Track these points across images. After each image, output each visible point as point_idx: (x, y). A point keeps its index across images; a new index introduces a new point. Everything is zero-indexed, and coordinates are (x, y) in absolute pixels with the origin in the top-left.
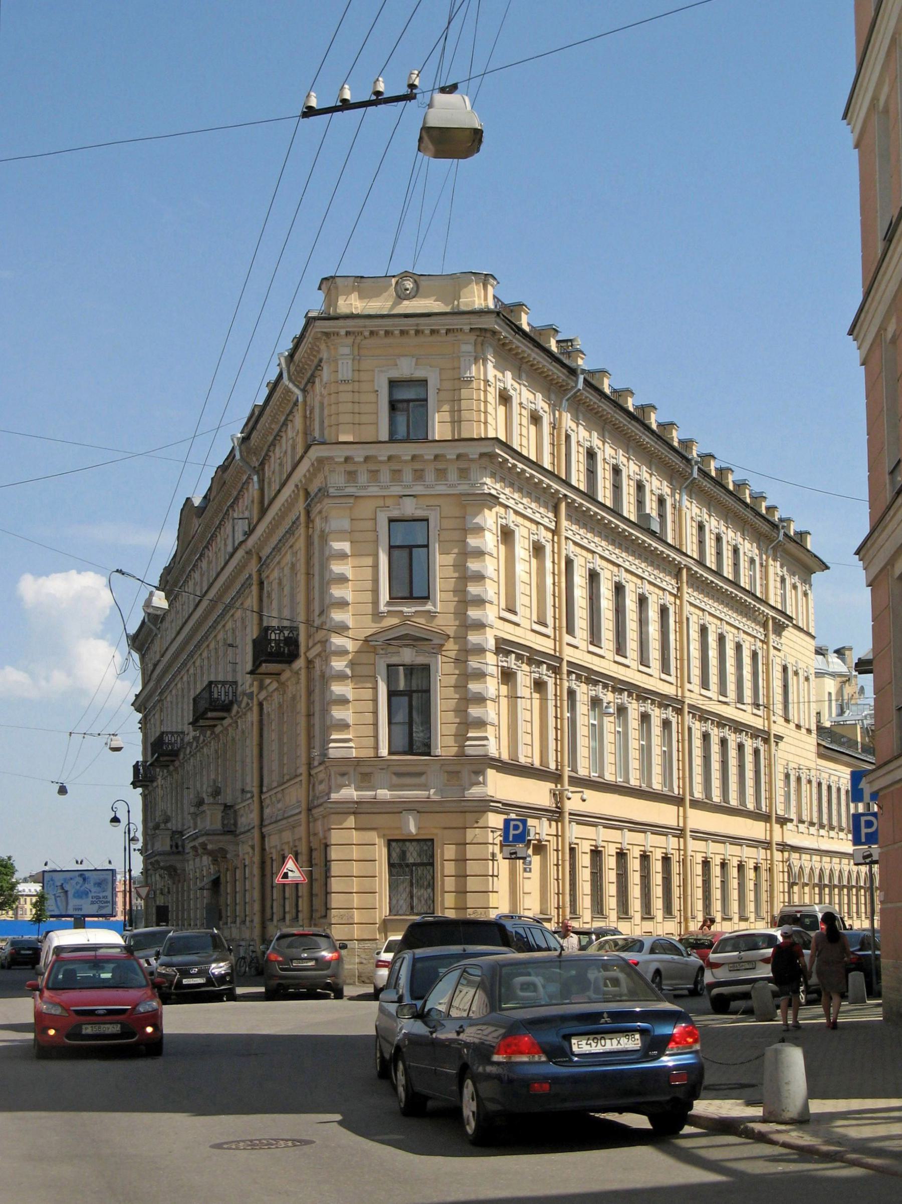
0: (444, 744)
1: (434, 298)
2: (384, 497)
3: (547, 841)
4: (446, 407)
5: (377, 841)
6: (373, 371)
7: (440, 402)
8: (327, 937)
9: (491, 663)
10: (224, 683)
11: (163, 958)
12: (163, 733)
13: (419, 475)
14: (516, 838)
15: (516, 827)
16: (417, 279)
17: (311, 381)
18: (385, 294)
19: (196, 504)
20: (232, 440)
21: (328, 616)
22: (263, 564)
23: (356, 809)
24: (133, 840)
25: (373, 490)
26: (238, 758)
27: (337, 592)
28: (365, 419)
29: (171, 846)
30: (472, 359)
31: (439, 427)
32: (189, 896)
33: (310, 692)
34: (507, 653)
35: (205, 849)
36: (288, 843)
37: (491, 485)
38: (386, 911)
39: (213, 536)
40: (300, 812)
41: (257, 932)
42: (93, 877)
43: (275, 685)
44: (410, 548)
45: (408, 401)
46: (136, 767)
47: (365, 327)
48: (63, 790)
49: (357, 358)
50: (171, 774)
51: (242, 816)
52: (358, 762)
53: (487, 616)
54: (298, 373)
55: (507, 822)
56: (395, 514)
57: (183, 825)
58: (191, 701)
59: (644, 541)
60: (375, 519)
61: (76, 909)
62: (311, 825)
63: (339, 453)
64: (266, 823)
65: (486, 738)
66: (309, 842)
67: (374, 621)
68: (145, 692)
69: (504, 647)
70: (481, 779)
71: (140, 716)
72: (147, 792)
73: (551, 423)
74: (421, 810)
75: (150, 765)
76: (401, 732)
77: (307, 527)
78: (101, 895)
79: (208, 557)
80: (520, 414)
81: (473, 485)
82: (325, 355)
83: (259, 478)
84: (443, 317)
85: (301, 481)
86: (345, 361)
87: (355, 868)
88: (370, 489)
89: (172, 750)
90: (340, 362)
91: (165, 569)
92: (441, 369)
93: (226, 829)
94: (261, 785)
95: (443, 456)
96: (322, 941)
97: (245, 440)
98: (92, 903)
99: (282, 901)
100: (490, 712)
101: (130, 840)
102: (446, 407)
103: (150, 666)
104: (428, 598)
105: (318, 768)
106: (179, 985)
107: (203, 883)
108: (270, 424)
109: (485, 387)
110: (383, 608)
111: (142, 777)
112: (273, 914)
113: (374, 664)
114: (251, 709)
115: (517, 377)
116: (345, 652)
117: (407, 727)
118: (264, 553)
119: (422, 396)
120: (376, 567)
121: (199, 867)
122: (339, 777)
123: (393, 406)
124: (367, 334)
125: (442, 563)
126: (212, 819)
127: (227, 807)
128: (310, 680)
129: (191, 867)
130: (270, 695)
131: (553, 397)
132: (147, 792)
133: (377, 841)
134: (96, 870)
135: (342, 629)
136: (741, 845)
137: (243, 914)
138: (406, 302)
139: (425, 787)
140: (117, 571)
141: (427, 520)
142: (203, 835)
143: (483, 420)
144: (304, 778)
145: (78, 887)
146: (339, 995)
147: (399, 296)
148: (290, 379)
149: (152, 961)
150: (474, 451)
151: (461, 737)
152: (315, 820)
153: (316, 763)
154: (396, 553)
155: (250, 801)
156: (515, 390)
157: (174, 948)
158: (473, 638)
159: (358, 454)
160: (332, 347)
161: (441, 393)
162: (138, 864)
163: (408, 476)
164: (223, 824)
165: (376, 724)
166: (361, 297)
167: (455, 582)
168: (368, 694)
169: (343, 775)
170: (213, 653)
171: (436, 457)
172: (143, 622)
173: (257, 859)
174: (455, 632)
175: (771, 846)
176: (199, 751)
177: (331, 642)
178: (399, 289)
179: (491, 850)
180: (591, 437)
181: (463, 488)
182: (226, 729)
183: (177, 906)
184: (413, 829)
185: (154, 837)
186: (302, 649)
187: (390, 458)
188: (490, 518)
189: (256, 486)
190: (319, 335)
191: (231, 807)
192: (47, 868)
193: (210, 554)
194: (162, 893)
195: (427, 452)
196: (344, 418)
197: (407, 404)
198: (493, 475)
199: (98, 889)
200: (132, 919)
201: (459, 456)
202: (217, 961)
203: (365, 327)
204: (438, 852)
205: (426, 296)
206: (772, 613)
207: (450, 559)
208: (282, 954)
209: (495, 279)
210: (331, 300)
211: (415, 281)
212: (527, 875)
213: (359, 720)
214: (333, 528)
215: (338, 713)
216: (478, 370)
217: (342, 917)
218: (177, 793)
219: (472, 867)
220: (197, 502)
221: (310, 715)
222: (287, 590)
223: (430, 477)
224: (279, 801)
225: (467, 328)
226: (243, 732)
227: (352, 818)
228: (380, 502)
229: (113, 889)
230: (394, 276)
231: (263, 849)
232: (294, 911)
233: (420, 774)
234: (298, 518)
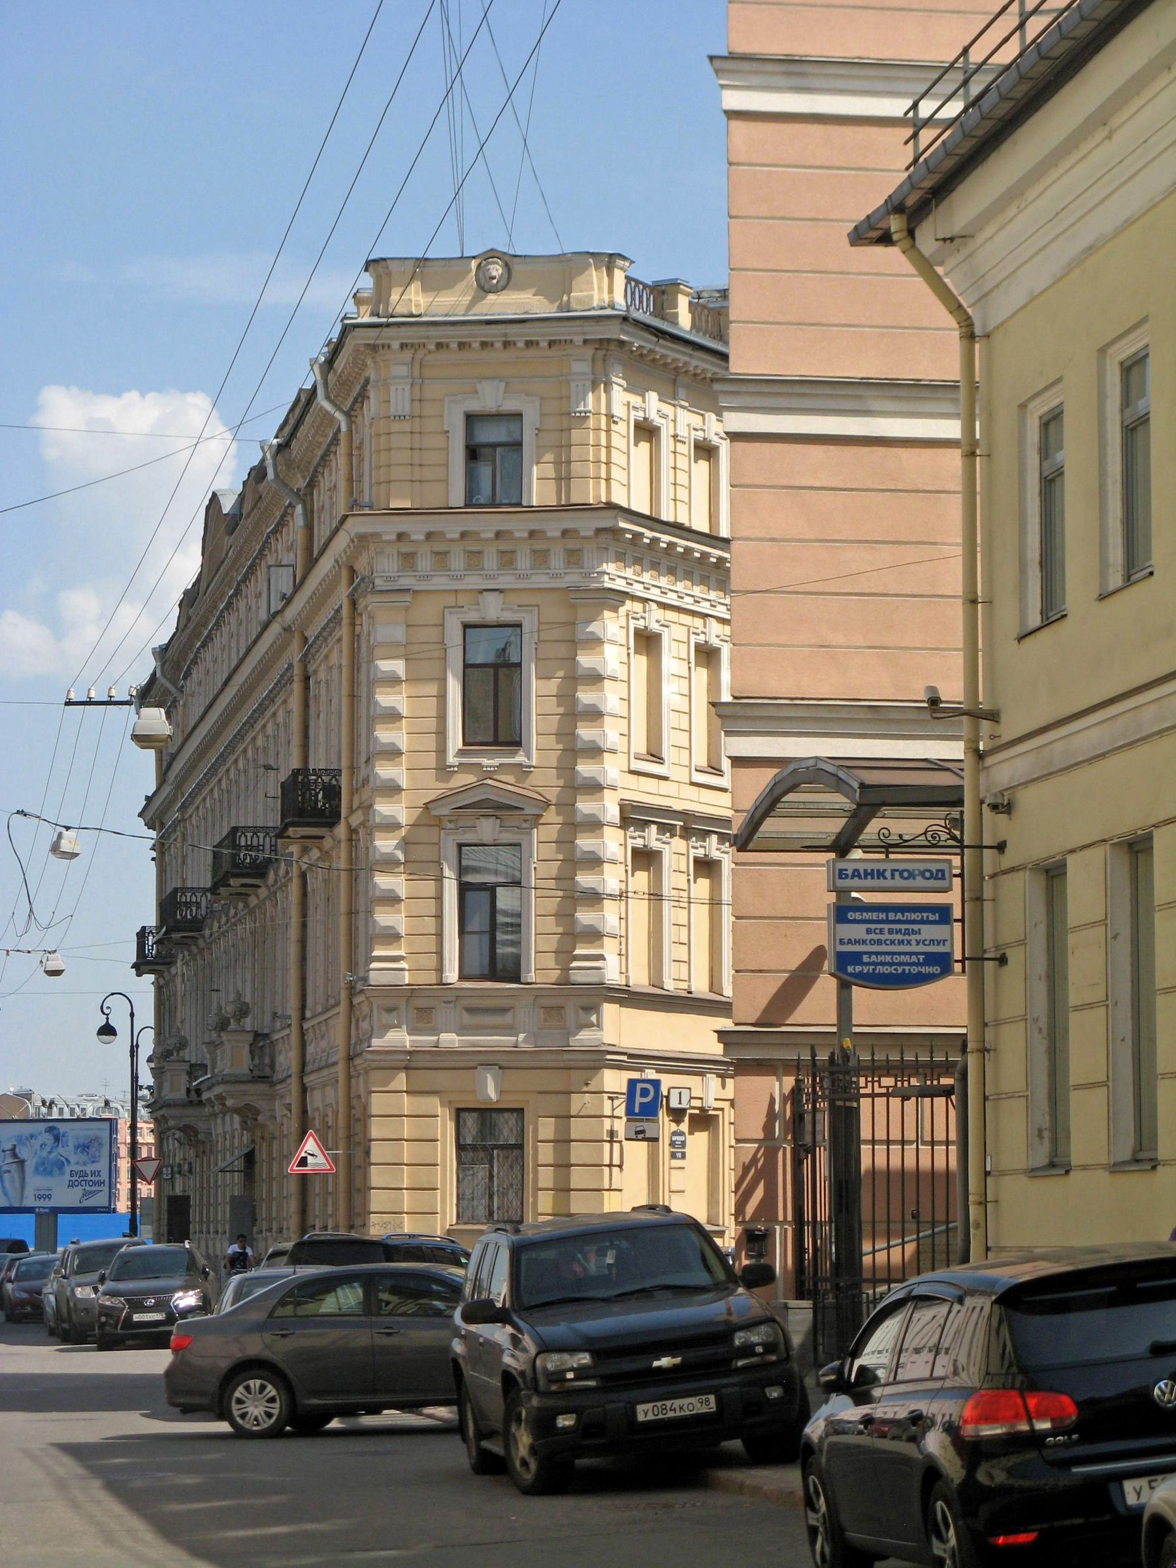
0: (539, 967)
1: (533, 290)
2: (456, 591)
3: (715, 1109)
4: (549, 457)
5: (439, 1111)
6: (442, 401)
7: (540, 450)
9: (614, 843)
13: (507, 559)
14: (644, 1105)
15: (645, 1093)
16: (508, 261)
18: (461, 286)
19: (225, 511)
20: (262, 448)
21: (373, 767)
23: (409, 1062)
25: (440, 582)
27: (384, 735)
29: (188, 1091)
30: (588, 384)
31: (539, 488)
37: (615, 574)
38: (451, 1217)
42: (73, 1133)
45: (494, 446)
47: (428, 338)
49: (418, 381)
51: (280, 1053)
52: (412, 992)
53: (605, 772)
54: (342, 385)
55: (632, 1083)
56: (473, 617)
60: (443, 625)
61: (40, 1197)
62: (353, 1081)
63: (389, 528)
64: (309, 1068)
65: (601, 957)
69: (633, 816)
70: (594, 1018)
74: (503, 1064)
77: (353, 624)
78: (89, 1169)
81: (587, 575)
83: (305, 509)
84: (544, 324)
86: (400, 387)
88: (435, 580)
89: (194, 918)
90: (393, 388)
91: (186, 593)
92: (542, 398)
93: (257, 1073)
94: (303, 1007)
95: (542, 532)
97: (282, 448)
98: (72, 1185)
100: (610, 916)
102: (549, 457)
103: (166, 759)
104: (519, 744)
106: (128, 1323)
108: (314, 437)
109: (608, 425)
110: (452, 759)
115: (669, 396)
116: (398, 826)
117: (486, 938)
118: (312, 632)
119: (516, 437)
120: (442, 697)
122: (383, 1013)
123: (473, 453)
124: (432, 347)
125: (539, 695)
129: (220, 1130)
132: (162, 982)
133: (439, 1111)
135: (392, 790)
138: (491, 297)
139: (510, 1030)
140: (18, 812)
141: (520, 626)
142: (219, 1083)
143: (603, 475)
145: (44, 1154)
148: (328, 397)
151: (565, 955)
154: (476, 674)
156: (665, 417)
158: (585, 806)
159: (417, 528)
160: (382, 364)
161: (541, 434)
163: (491, 561)
165: (439, 935)
166: (425, 289)
167: (560, 721)
169: (390, 1010)
181: (573, 579)
182: (263, 901)
184: (492, 1093)
187: (463, 535)
188: (614, 627)
190: (362, 349)
195: (519, 526)
196: (396, 473)
197: (491, 452)
198: (620, 558)
199: (84, 1157)
202: (186, 1288)
203: (428, 338)
205: (522, 288)
207: (552, 686)
209: (625, 258)
212: (676, 1163)
213: (413, 931)
214: (379, 639)
215: (384, 918)
216: (598, 400)
223: (523, 561)
227: (402, 1076)
228: (450, 600)
230: (474, 257)
233: (503, 1010)
234: (341, 607)
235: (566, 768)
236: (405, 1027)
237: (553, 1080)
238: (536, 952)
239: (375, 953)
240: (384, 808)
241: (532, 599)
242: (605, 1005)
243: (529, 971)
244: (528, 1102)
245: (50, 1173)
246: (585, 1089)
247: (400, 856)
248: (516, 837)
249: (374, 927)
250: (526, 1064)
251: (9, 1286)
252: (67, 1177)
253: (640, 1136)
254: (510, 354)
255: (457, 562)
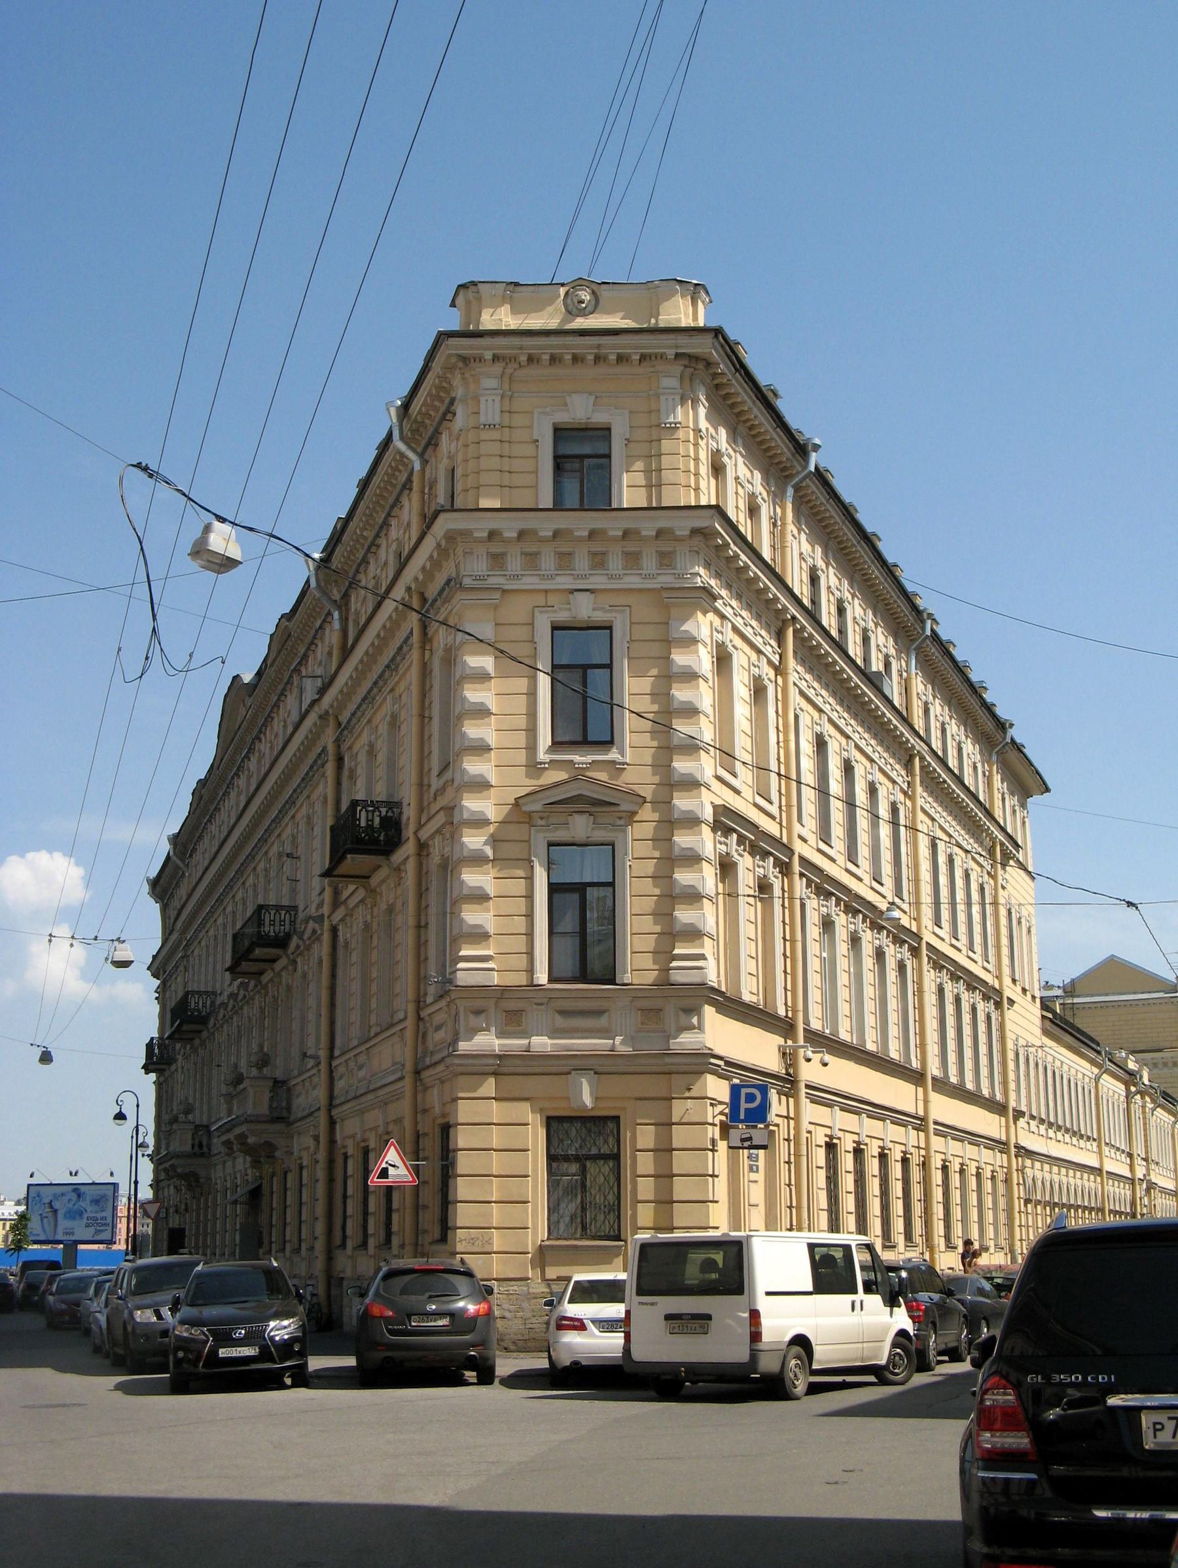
0: (637, 965)
1: (621, 314)
2: (546, 591)
4: (639, 465)
5: (530, 1118)
8: (469, 1274)
10: (278, 908)
11: (186, 1311)
12: (187, 993)
15: (750, 1098)
16: (596, 288)
17: (433, 442)
18: (550, 309)
22: (344, 729)
23: (499, 1066)
24: (143, 1145)
25: (530, 581)
26: (296, 1013)
28: (517, 480)
30: (678, 398)
31: (629, 490)
32: (214, 1214)
33: (421, 892)
34: (728, 831)
35: (244, 1144)
36: (376, 1128)
39: (269, 719)
40: (402, 1078)
41: (319, 1265)
43: (361, 893)
44: (585, 668)
46: (150, 1046)
47: (521, 348)
48: (46, 1058)
49: (507, 396)
50: (194, 1050)
51: (298, 1096)
52: (503, 992)
56: (562, 616)
57: (209, 1117)
58: (229, 938)
59: (877, 707)
60: (532, 624)
62: (419, 1097)
65: (702, 957)
66: (416, 1123)
67: (528, 776)
68: (163, 953)
69: (726, 821)
70: (695, 1020)
71: (157, 982)
72: (162, 1079)
73: (771, 518)
74: (600, 1069)
75: (168, 1038)
76: (569, 946)
77: (423, 649)
78: (99, 1215)
79: (260, 751)
80: (737, 493)
81: (680, 577)
82: (459, 392)
85: (416, 579)
86: (490, 399)
87: (496, 1163)
92: (631, 412)
94: (332, 1048)
96: (461, 1283)
98: (87, 1226)
99: (360, 1218)
100: (709, 917)
101: (137, 1147)
102: (639, 465)
103: (173, 914)
105: (438, 997)
107: (235, 1197)
110: (542, 756)
111: (158, 1059)
112: (344, 1237)
113: (528, 841)
114: (318, 939)
115: (733, 436)
116: (485, 822)
117: (577, 940)
118: (344, 717)
120: (532, 694)
121: (232, 1172)
122: (471, 1016)
123: (560, 464)
124: (523, 358)
125: (634, 688)
126: (256, 1101)
127: (277, 1084)
128: (421, 874)
130: (350, 914)
131: (772, 482)
134: (94, 1184)
135: (481, 785)
136: (978, 1145)
137: (296, 1240)
140: (138, 466)
141: (610, 628)
144: (410, 1023)
146: (486, 1376)
147: (569, 312)
148: (402, 438)
149: (166, 1312)
150: (682, 525)
151: (663, 955)
152: (426, 1089)
153: (429, 999)
155: (314, 1071)
157: (205, 1292)
158: (682, 803)
161: (631, 445)
162: (146, 1171)
164: (271, 1107)
165: (530, 935)
166: (515, 311)
168: (519, 887)
169: (478, 1012)
170: (261, 879)
171: (626, 534)
172: (168, 858)
173: (322, 1155)
174: (654, 792)
175: (1009, 1148)
176: (236, 1012)
177: (462, 807)
178: (569, 301)
179: (710, 1135)
180: (813, 551)
181: (666, 580)
182: (279, 975)
183: (198, 1228)
185: (170, 1133)
186: (409, 832)
187: (557, 534)
188: (703, 625)
189: (337, 625)
190: (453, 360)
191: (284, 1082)
192: (34, 1181)
193: (262, 747)
194: (176, 1211)
195: (613, 525)
196: (485, 478)
197: (581, 460)
198: (707, 566)
199: (96, 1208)
200: (136, 1245)
201: (660, 533)
202: (278, 1315)
204: (626, 1135)
205: (609, 312)
206: (1001, 837)
207: (645, 684)
208: (390, 1303)
209: (707, 293)
210: (472, 313)
211: (593, 292)
213: (502, 929)
215: (472, 916)
217: (472, 1241)
218: (203, 1075)
219: (681, 1162)
220: (247, 678)
221: (421, 927)
222: (381, 757)
223: (615, 563)
224: (360, 1067)
225: (671, 353)
226: (304, 975)
227: (491, 1081)
228: (540, 600)
229: (115, 1208)
231: (332, 1142)
232: (382, 1234)
233: (599, 1013)
234: (411, 633)
235: (662, 766)
236: (493, 1029)
237: (653, 1086)
238: (633, 953)
239: (462, 953)
240: (472, 804)
241: (621, 600)
242: (706, 1006)
243: (625, 972)
244: (624, 1109)
245: (74, 1218)
246: (687, 1094)
247: (489, 852)
248: (610, 834)
249: (461, 927)
250: (621, 1069)
251: (51, 1298)
252: (85, 1221)
253: (746, 1144)
254: (602, 369)
255: (548, 562)
